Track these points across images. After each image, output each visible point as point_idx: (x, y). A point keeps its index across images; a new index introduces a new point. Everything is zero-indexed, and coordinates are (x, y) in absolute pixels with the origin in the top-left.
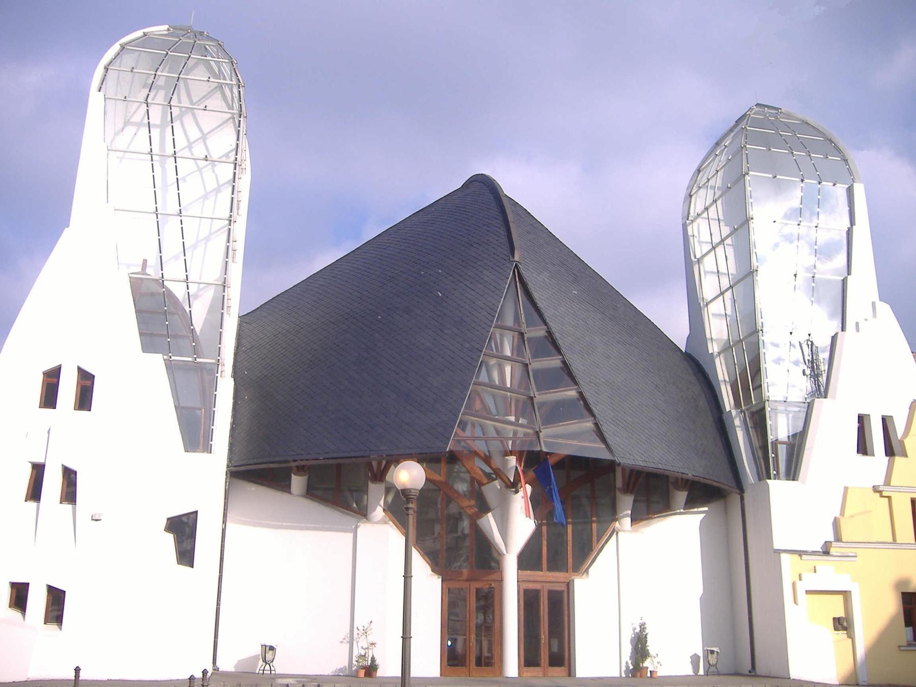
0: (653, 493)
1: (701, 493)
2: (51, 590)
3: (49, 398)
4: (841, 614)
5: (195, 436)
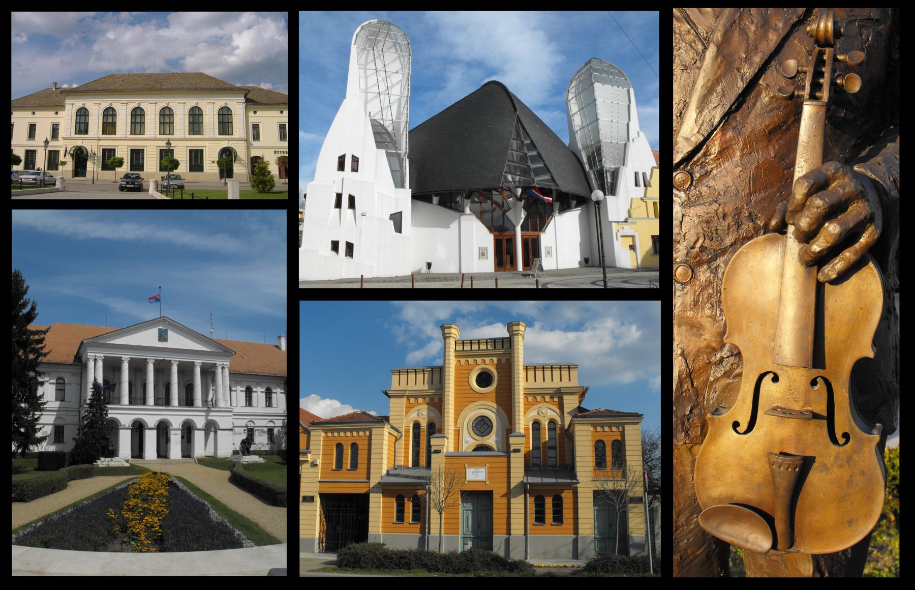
0: (566, 202)
1: (582, 201)
2: (347, 243)
3: (341, 167)
4: (631, 243)
5: (399, 184)
